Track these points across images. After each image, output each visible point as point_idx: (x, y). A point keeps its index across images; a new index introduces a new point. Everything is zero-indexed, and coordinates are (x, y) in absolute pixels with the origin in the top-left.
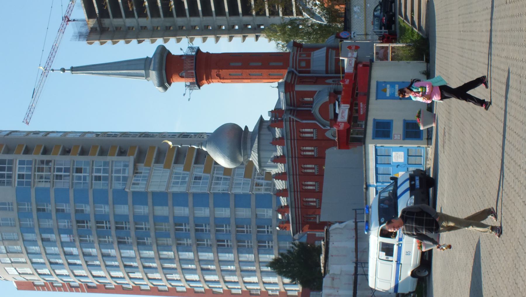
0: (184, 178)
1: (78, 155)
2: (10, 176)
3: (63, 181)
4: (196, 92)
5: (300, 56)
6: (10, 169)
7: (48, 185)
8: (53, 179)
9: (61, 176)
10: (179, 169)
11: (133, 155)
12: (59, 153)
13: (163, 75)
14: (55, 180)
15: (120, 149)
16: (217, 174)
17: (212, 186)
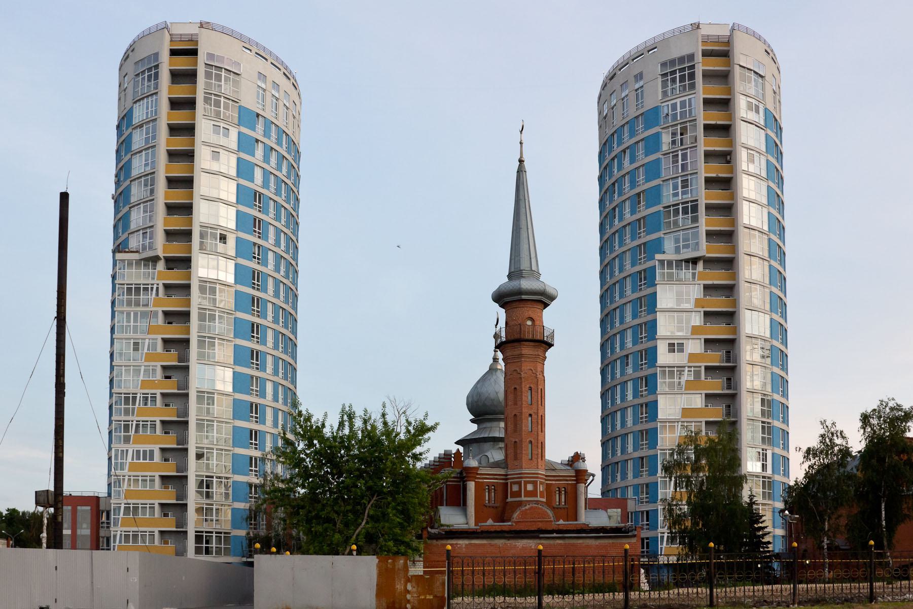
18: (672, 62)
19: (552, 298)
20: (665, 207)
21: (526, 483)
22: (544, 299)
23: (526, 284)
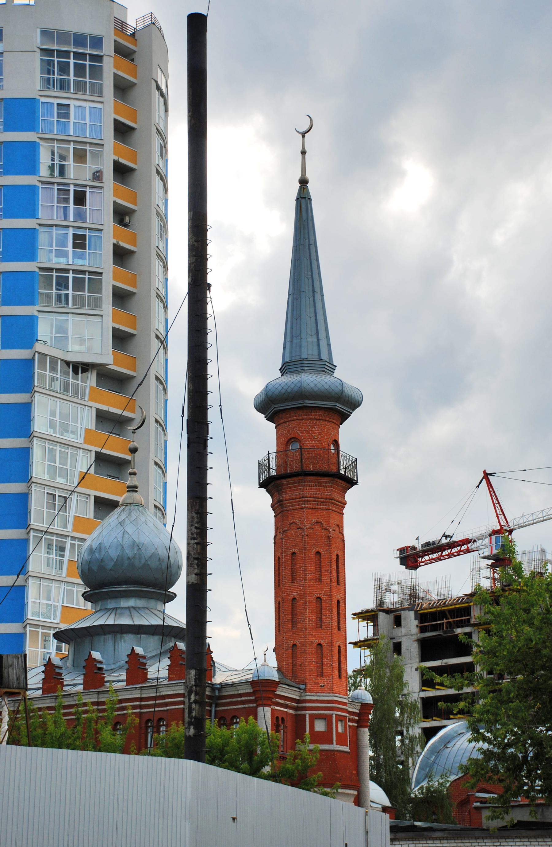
0: (64, 473)
1: (113, 116)
2: (63, 85)
3: (56, 204)
4: (254, 477)
5: (340, 719)
6: (80, 87)
7: (44, 171)
8: (58, 184)
9: (67, 201)
10: (84, 462)
11: (115, 363)
12: (117, 326)
13: (318, 707)
14: (56, 187)
15: (130, 336)
16: (73, 545)
17: (40, 630)
18: (63, 36)
19: (354, 404)
20: (41, 269)
21: (313, 718)
22: (340, 406)
23: (310, 380)
